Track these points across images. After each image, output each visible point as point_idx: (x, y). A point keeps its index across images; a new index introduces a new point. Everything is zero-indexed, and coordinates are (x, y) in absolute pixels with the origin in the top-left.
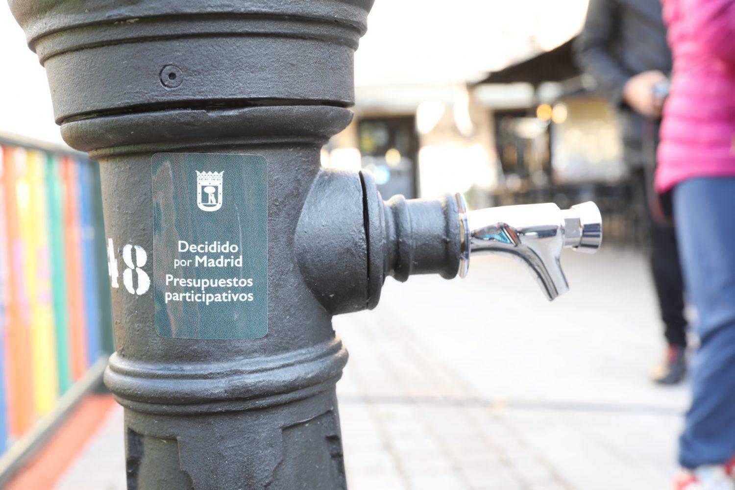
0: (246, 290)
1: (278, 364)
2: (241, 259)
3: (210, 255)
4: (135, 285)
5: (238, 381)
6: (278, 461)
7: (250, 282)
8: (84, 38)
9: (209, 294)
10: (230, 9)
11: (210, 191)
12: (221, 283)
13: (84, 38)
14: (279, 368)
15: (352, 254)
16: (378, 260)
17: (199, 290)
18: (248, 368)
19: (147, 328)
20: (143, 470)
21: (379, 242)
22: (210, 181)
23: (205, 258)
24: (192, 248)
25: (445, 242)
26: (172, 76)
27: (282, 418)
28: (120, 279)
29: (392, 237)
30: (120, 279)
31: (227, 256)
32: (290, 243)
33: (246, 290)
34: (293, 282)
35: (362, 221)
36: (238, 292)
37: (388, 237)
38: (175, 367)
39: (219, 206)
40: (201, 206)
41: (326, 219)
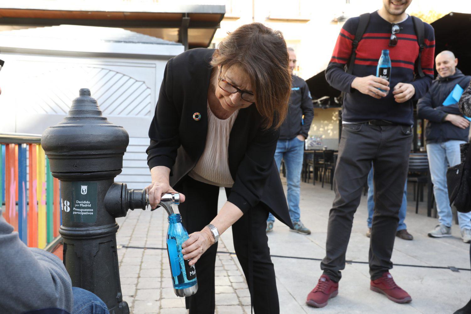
0: (91, 212)
1: (98, 229)
2: (90, 205)
3: (83, 204)
4: (67, 210)
5: (88, 232)
6: (97, 251)
7: (92, 210)
8: (58, 157)
9: (83, 212)
10: (89, 154)
11: (84, 190)
12: (86, 210)
13: (58, 157)
14: (98, 230)
15: (118, 204)
16: (124, 206)
17: (80, 212)
18: (91, 229)
19: (70, 219)
20: (67, 253)
21: (124, 202)
22: (84, 188)
23: (82, 204)
24: (80, 202)
26: (76, 166)
27: (99, 241)
28: (64, 208)
29: (129, 200)
30: (64, 208)
31: (87, 204)
32: (103, 201)
33: (91, 212)
34: (103, 210)
35: (120, 197)
36: (89, 212)
38: (74, 228)
39: (86, 193)
40: (82, 193)
41: (112, 195)
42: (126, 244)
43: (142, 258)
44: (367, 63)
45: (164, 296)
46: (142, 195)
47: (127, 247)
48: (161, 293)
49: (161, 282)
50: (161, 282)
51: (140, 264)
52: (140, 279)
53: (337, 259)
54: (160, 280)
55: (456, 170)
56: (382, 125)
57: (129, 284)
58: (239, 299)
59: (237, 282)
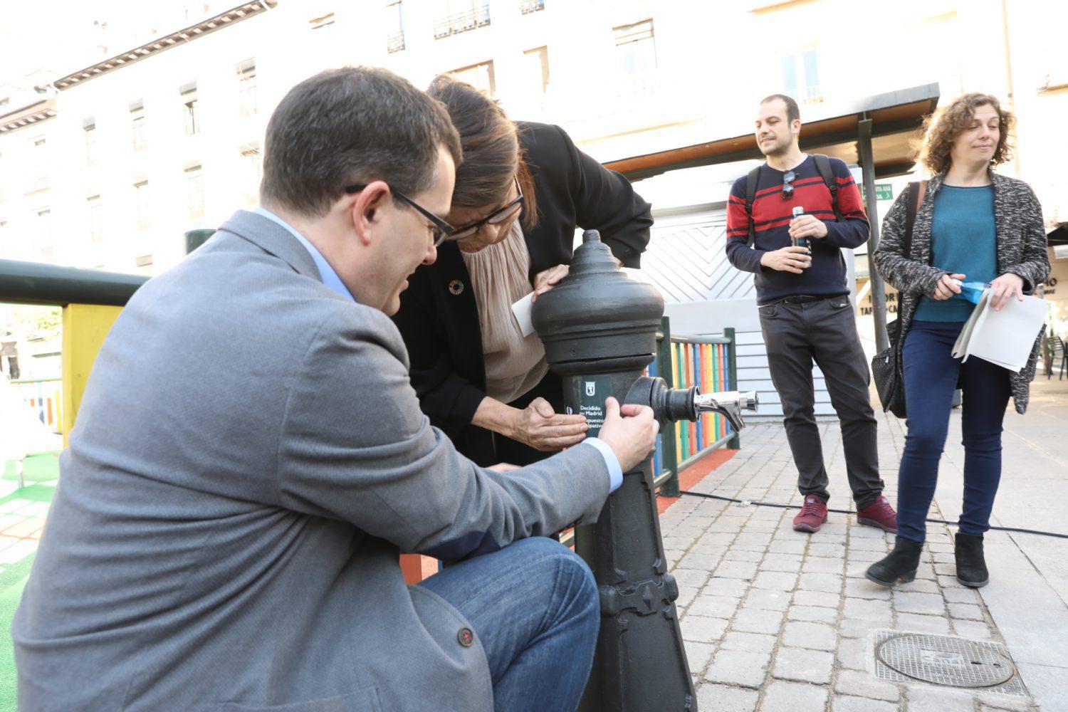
3: (591, 411)
11: (590, 389)
12: (594, 421)
24: (585, 408)
25: (686, 408)
29: (665, 405)
31: (596, 411)
37: (662, 405)
39: (593, 394)
40: (587, 394)
42: (757, 499)
43: (779, 522)
44: (767, 227)
45: (802, 584)
46: (687, 395)
47: (758, 504)
48: (798, 580)
49: (803, 562)
50: (803, 562)
51: (773, 531)
52: (768, 555)
53: (817, 476)
54: (801, 558)
55: (885, 358)
56: (802, 302)
57: (748, 561)
58: (946, 606)
59: (949, 576)
